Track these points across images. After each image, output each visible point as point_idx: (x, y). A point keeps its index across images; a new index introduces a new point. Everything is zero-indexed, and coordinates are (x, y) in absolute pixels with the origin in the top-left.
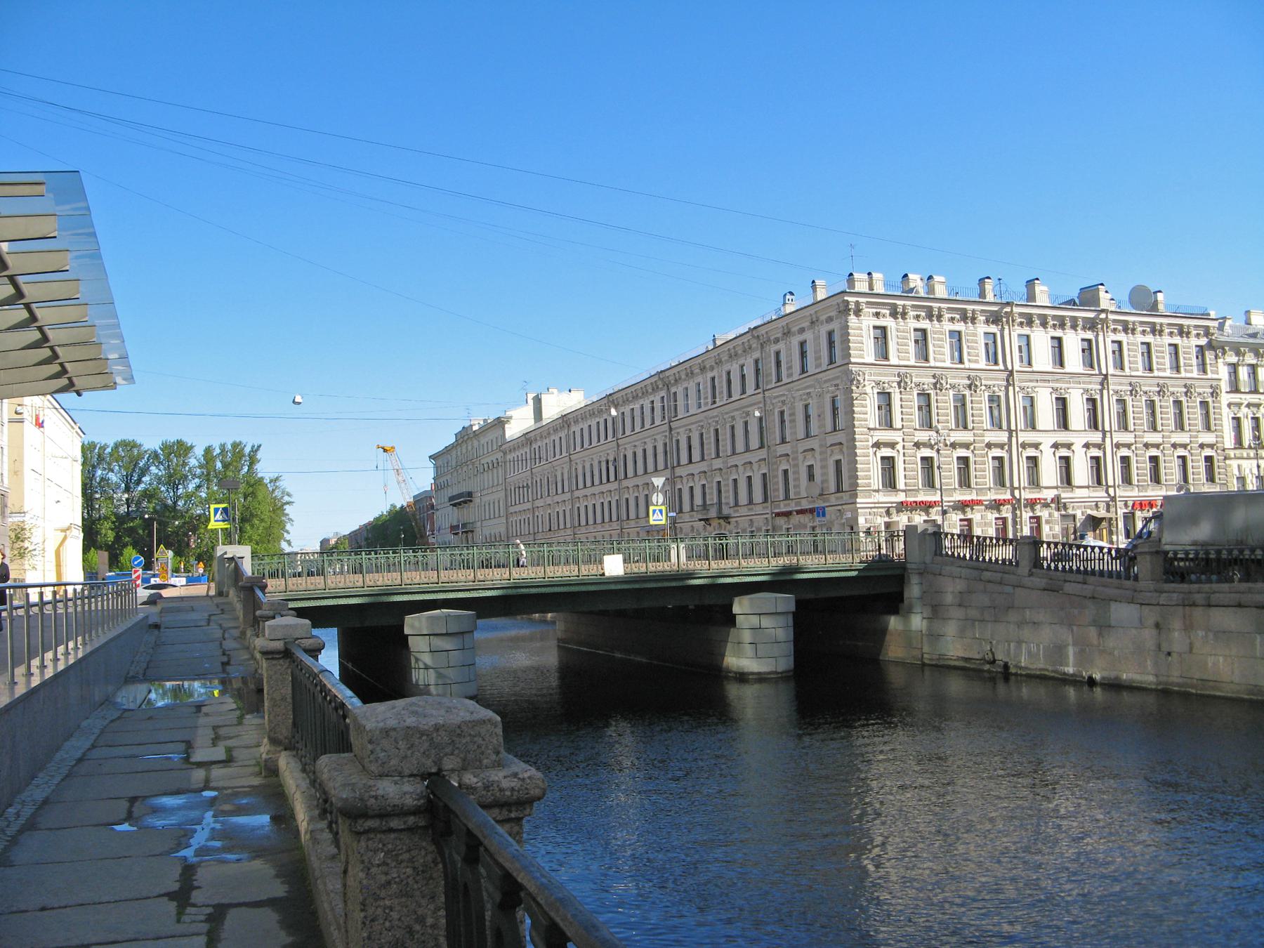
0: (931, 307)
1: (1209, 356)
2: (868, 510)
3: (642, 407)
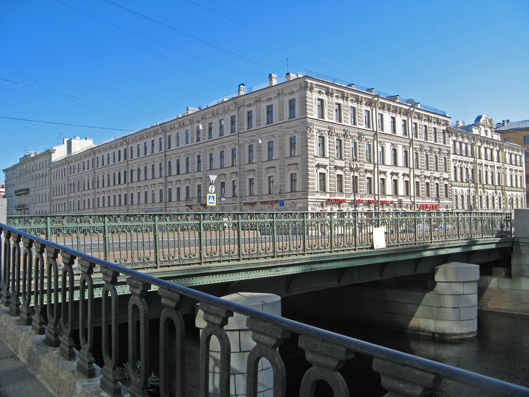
0: (344, 92)
1: (447, 135)
2: (312, 203)
3: (120, 151)
